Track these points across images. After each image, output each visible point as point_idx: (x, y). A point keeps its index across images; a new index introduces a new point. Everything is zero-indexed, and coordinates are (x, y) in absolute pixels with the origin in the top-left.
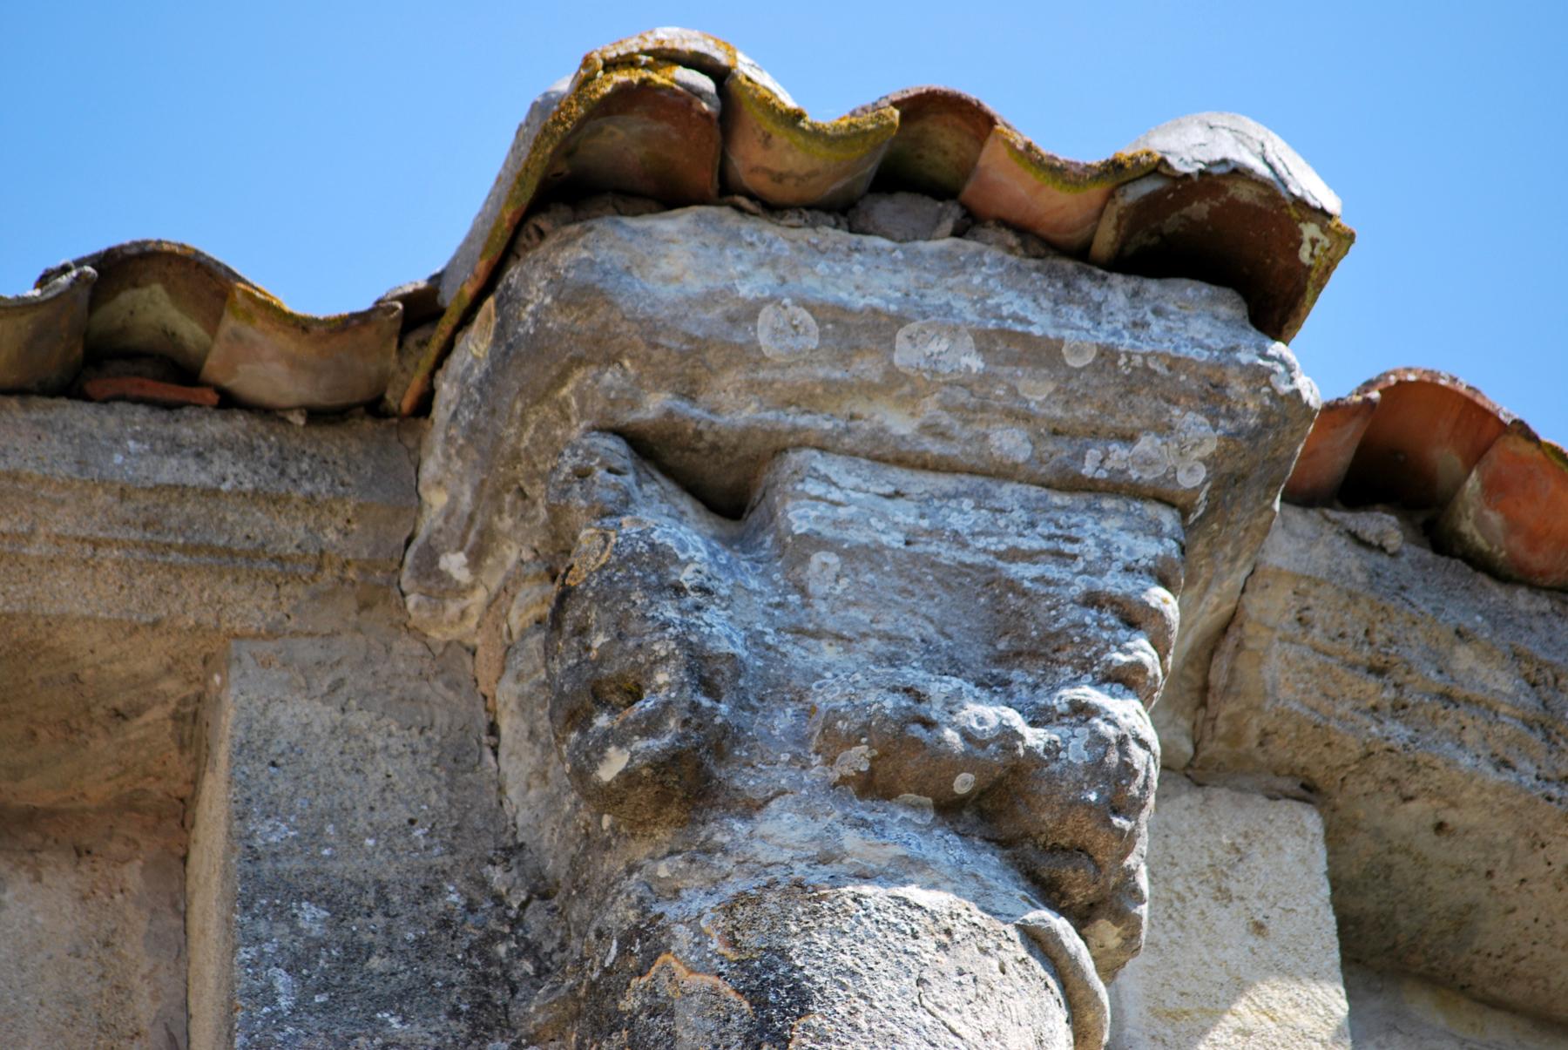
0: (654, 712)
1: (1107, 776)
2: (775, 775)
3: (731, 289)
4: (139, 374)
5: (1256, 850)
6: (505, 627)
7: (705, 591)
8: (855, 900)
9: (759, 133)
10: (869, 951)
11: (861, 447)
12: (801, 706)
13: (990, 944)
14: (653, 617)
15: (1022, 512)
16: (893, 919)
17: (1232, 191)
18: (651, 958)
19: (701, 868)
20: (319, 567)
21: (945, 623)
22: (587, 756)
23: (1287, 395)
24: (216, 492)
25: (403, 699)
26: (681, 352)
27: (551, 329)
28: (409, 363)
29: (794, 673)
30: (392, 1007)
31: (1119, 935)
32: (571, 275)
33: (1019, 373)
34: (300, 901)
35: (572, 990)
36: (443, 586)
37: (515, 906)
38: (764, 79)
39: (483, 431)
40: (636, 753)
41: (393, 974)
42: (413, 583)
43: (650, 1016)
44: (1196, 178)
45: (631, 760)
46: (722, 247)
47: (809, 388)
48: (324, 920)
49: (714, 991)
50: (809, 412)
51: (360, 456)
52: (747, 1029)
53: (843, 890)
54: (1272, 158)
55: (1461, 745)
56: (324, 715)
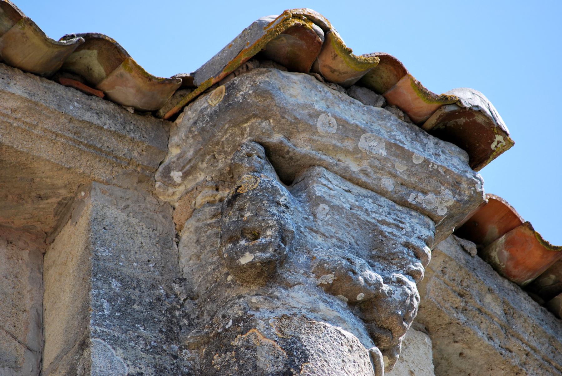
0: (266, 244)
1: (405, 306)
2: (298, 277)
3: (312, 105)
4: (76, 80)
5: (411, 346)
6: (194, 202)
7: (287, 207)
8: (324, 327)
9: (333, 54)
10: (328, 346)
11: (339, 171)
12: (309, 255)
13: (362, 355)
14: (270, 211)
15: (387, 208)
16: (335, 337)
17: (476, 117)
18: (247, 329)
19: (269, 302)
20: (129, 164)
21: (358, 240)
22: (236, 253)
23: (479, 192)
24: (102, 128)
25: (148, 218)
26: (291, 122)
27: (249, 102)
28: (175, 101)
29: (308, 243)
30: (141, 323)
31: (388, 363)
32: (262, 85)
33: (397, 160)
34: (112, 278)
35: (207, 333)
36: (170, 182)
37: (182, 299)
38: (338, 35)
39: (208, 132)
40: (257, 257)
41: (141, 312)
42: (160, 178)
43: (246, 349)
44: (468, 110)
45: (254, 259)
46: (311, 90)
47: (328, 146)
48: (120, 287)
49: (273, 346)
50: (325, 155)
51: (150, 129)
52: (285, 362)
53: (320, 323)
54: (492, 110)
55: (479, 328)
56: (122, 216)
